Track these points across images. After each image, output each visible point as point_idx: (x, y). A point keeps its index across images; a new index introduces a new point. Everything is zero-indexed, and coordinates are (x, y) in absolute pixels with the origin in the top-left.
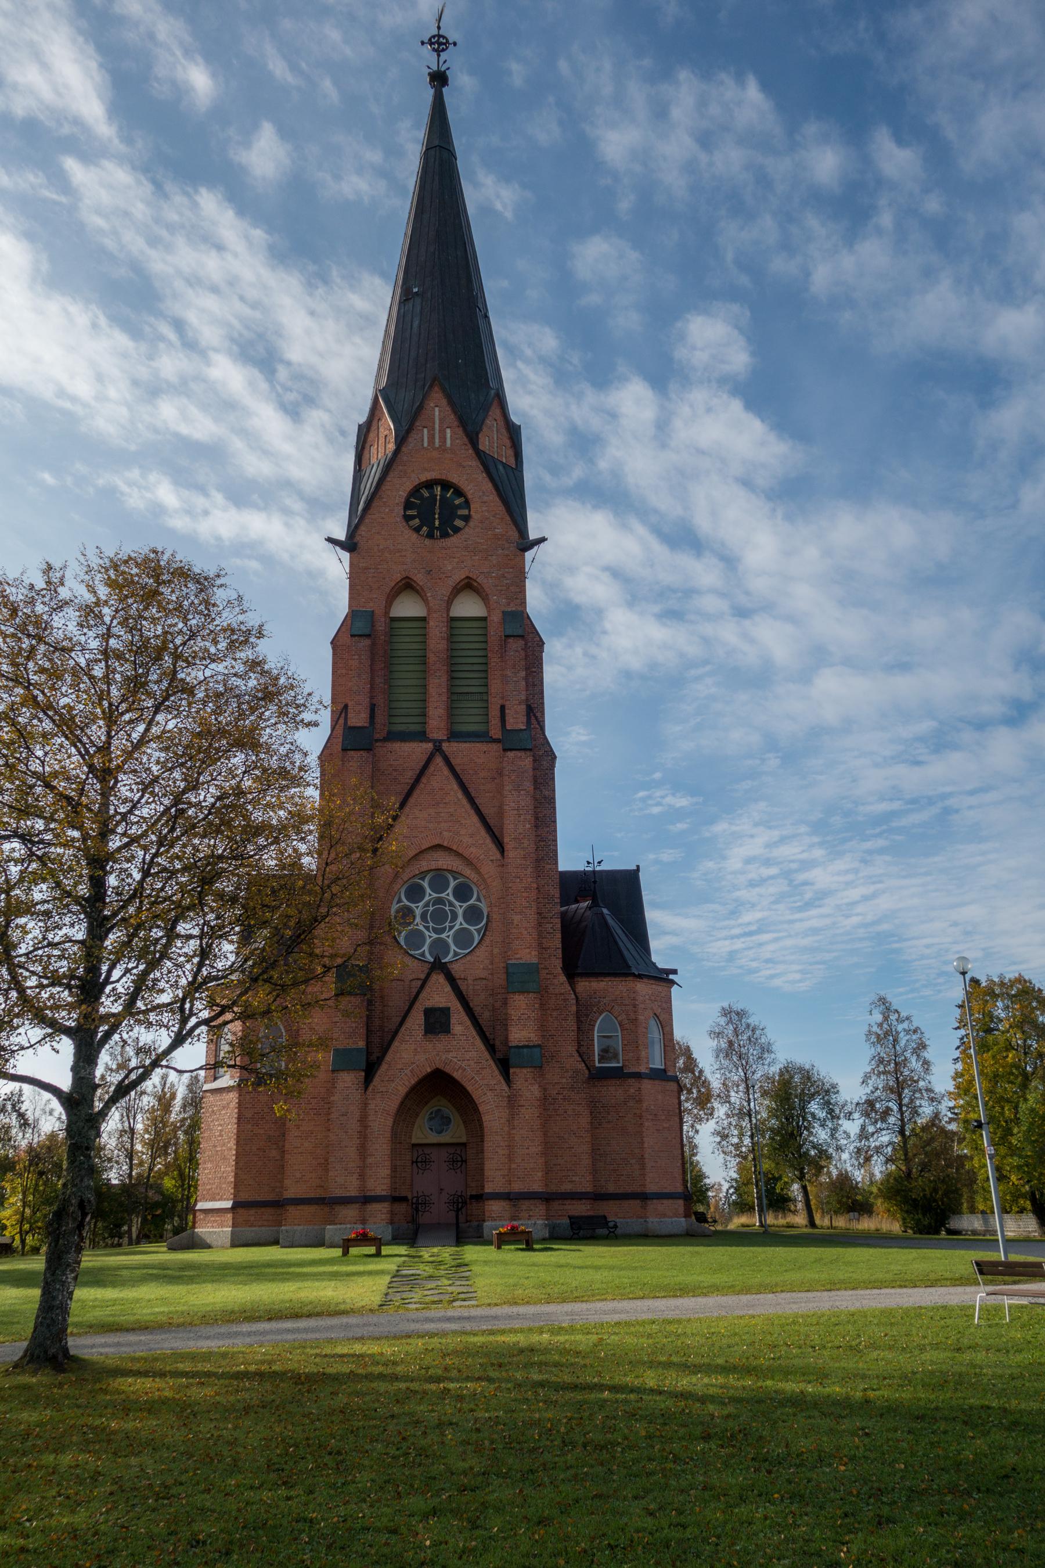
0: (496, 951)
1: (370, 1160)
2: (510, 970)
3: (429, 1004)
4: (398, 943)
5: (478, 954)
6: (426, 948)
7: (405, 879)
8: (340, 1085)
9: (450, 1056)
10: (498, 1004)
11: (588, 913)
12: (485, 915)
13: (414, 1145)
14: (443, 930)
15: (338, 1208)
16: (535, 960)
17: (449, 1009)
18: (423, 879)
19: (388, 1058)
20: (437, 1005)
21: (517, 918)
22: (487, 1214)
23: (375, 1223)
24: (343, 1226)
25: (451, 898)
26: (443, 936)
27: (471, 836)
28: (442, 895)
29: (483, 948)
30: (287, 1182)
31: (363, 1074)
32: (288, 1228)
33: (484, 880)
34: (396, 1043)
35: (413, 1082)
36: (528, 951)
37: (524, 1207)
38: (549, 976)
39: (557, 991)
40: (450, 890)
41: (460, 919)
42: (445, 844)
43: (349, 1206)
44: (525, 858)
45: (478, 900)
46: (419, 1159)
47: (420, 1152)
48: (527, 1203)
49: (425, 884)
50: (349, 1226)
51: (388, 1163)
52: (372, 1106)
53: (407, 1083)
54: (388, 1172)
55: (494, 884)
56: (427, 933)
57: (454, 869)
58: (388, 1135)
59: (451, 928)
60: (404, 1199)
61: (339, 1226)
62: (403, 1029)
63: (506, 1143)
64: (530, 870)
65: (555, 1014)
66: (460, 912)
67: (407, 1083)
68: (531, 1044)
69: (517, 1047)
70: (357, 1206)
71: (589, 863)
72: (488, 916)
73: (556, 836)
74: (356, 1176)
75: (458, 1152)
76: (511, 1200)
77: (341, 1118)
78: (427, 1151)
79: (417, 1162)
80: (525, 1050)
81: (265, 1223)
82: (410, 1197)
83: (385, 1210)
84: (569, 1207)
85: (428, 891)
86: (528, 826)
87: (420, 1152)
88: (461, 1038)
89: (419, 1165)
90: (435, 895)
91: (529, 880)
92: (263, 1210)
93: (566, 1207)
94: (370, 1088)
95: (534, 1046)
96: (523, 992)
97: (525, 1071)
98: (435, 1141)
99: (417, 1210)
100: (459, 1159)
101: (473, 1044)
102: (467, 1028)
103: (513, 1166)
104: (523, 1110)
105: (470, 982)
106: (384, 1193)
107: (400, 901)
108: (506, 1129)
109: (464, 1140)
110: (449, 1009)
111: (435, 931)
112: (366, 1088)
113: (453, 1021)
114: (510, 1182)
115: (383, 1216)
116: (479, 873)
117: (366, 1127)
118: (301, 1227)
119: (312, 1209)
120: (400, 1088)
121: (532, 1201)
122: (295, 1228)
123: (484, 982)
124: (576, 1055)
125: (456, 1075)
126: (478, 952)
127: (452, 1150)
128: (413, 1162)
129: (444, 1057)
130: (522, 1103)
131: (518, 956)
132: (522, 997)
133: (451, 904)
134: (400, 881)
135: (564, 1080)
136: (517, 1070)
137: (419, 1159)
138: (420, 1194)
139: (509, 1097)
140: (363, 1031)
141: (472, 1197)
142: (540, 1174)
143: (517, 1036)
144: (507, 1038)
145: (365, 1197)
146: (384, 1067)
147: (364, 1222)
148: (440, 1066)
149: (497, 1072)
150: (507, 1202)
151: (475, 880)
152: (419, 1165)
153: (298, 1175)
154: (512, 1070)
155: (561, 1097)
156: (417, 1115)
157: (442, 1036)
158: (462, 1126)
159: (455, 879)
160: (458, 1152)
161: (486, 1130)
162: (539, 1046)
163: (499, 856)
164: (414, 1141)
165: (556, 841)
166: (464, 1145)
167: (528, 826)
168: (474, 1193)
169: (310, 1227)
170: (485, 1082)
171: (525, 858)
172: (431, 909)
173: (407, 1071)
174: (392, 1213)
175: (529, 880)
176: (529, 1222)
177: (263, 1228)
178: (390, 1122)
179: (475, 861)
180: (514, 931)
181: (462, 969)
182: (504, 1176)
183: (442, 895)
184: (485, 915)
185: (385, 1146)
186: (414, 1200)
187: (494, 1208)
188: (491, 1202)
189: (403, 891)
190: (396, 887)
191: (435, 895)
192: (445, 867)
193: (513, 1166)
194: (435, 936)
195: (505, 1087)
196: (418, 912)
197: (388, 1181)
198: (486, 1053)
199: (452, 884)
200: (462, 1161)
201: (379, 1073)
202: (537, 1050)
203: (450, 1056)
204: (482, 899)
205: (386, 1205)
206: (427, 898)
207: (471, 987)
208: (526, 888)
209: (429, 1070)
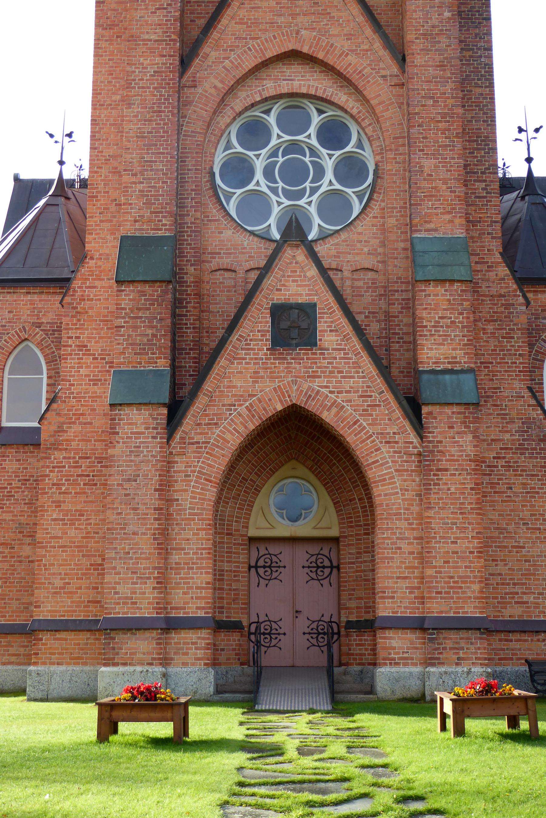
0: (392, 221)
1: (175, 558)
2: (418, 248)
3: (279, 298)
4: (228, 214)
5: (360, 229)
6: (272, 221)
7: (238, 108)
8: (124, 430)
9: (316, 385)
10: (396, 309)
11: (520, 204)
12: (371, 168)
13: (252, 540)
14: (300, 195)
15: (119, 637)
16: (460, 233)
17: (315, 305)
18: (267, 112)
19: (208, 386)
20: (293, 300)
21: (428, 164)
22: (382, 654)
23: (185, 664)
24: (131, 669)
25: (314, 142)
26: (302, 202)
27: (349, 37)
28: (300, 138)
29: (368, 220)
30: (40, 594)
31: (165, 411)
32: (40, 668)
33: (372, 110)
34: (222, 362)
35: (252, 427)
36: (448, 217)
37: (449, 644)
38: (479, 267)
39: (494, 291)
40: (312, 130)
41: (329, 175)
42: (305, 50)
43: (139, 634)
44: (441, 66)
45: (360, 145)
46: (261, 563)
47: (262, 552)
48: (453, 635)
49: (272, 120)
50: (139, 668)
51: (207, 564)
52: (179, 466)
53: (241, 429)
54: (209, 578)
55: (387, 114)
56: (274, 198)
57: (320, 93)
58: (208, 515)
59: (314, 191)
60: (235, 626)
61: (121, 669)
62: (234, 338)
63: (415, 534)
64: (450, 86)
65: (490, 328)
66: (329, 165)
67: (241, 429)
68: (458, 368)
69: (433, 372)
70: (154, 634)
71: (520, 130)
72: (376, 172)
73: (490, 42)
74: (151, 583)
75: (325, 552)
76: (423, 629)
77: (126, 485)
78: (274, 549)
79: (256, 567)
80: (447, 377)
81: (13, 659)
82: (245, 623)
83: (202, 643)
84: (518, 645)
85: (276, 130)
86: (447, 14)
87: (262, 552)
88: (335, 354)
89: (261, 571)
90: (287, 138)
91: (450, 102)
92: (9, 638)
93: (512, 645)
94: (178, 436)
95: (462, 371)
96: (443, 281)
97: (448, 410)
98: (286, 533)
99: (258, 644)
100: (327, 563)
101: (356, 365)
102: (346, 338)
103: (430, 572)
104: (445, 477)
105: (346, 274)
106: (201, 614)
107: (229, 145)
108: (415, 509)
109: (334, 532)
110: (315, 305)
111: (288, 195)
112: (170, 437)
113: (321, 326)
114: (422, 599)
115: (200, 653)
116: (365, 100)
117: (170, 501)
118: (62, 668)
119: (83, 638)
120: (228, 436)
121: (463, 634)
122: (53, 668)
123: (370, 275)
124: (527, 394)
125: (327, 417)
126: (359, 227)
127: (314, 549)
128: (250, 567)
129: (305, 386)
130: (444, 464)
131: (432, 226)
132: (440, 290)
133: (313, 152)
134: (229, 113)
135: (507, 436)
136: (436, 409)
137: (261, 563)
138: (326, 582)
139: (419, 454)
140: (166, 342)
141: (350, 625)
142: (476, 587)
143: (431, 354)
144: (415, 360)
145: (168, 620)
146: (201, 400)
147: (165, 661)
148: (301, 401)
149: (398, 413)
150: (418, 634)
151: (355, 111)
152: (261, 571)
153: (58, 583)
154: (425, 410)
155: (502, 462)
156: (258, 491)
157: (301, 352)
158: (332, 509)
159: (320, 112)
160: (325, 552)
161: (378, 511)
162: (471, 371)
163: (395, 70)
164: (253, 532)
165: (490, 49)
166: (336, 540)
167: (447, 14)
168: (353, 618)
169: (77, 668)
170: (378, 429)
171: (441, 66)
172: (281, 160)
173: (242, 409)
174: (215, 647)
175: (450, 102)
176: (459, 669)
177: (10, 667)
178: (211, 493)
179: (354, 78)
180: (425, 184)
181: (333, 252)
182: (412, 589)
183: (300, 138)
184: (371, 168)
185: (202, 534)
186: (253, 628)
187: (394, 643)
188: (389, 633)
189: (234, 130)
190: (222, 121)
191: (287, 138)
192: (304, 90)
193: (430, 572)
194: (287, 203)
195: (413, 437)
196: (259, 165)
197: (207, 593)
198: (379, 380)
199: (316, 120)
200: (332, 567)
201: (192, 411)
202: (468, 378)
203: (316, 385)
204: (366, 143)
205: (204, 633)
206: (274, 141)
207: (348, 283)
208: (444, 116)
209: (279, 408)
